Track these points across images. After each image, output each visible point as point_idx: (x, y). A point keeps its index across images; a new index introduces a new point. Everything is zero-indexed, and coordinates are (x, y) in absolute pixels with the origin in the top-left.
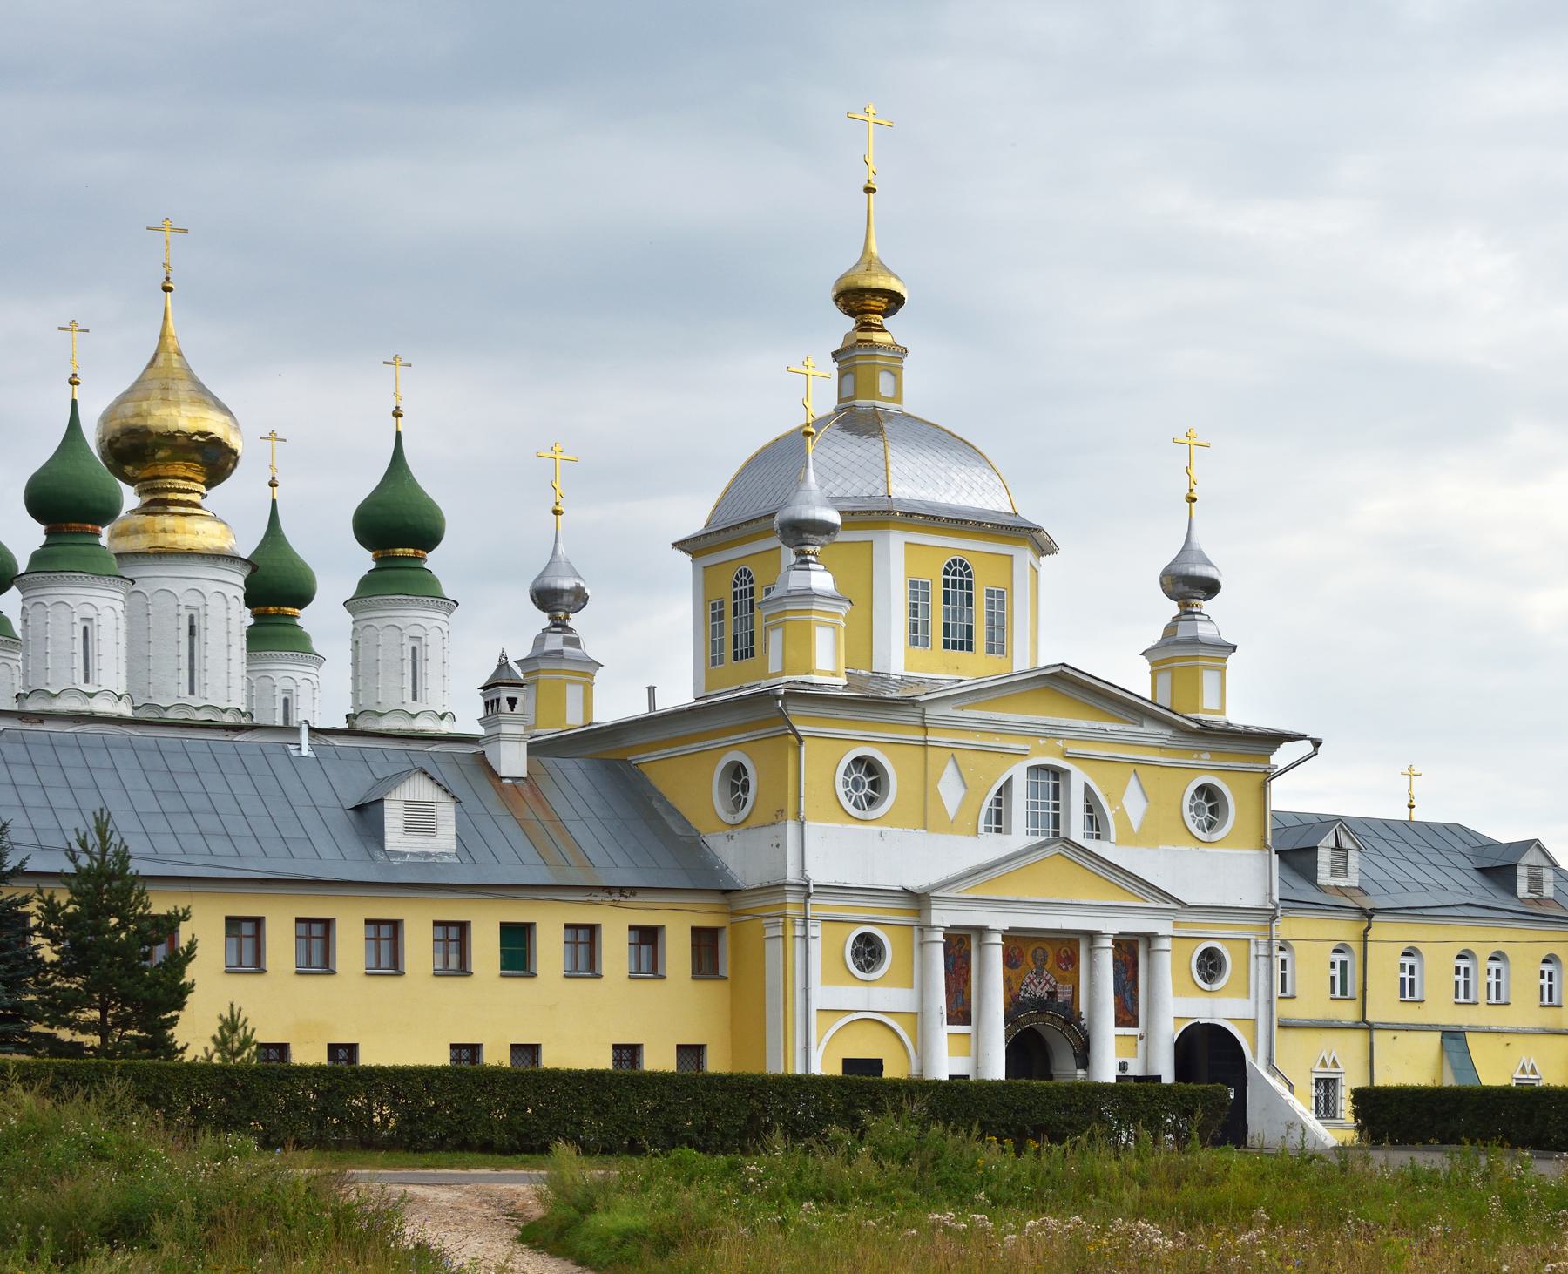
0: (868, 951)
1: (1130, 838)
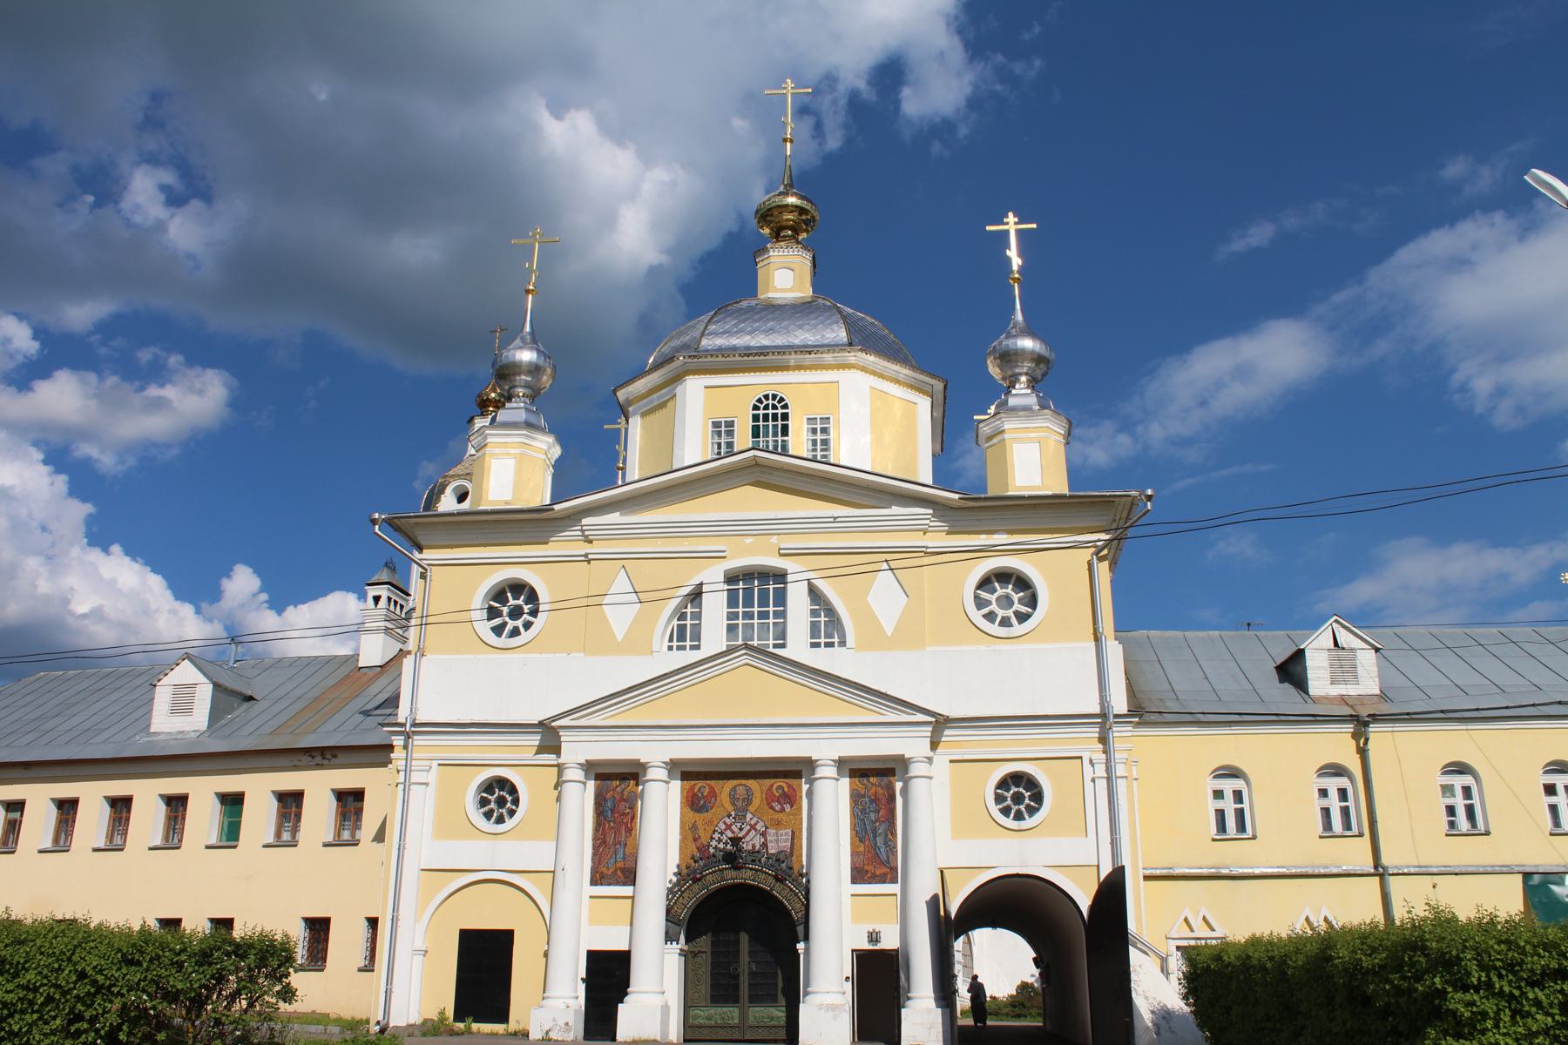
0: (499, 797)
1: (876, 640)
